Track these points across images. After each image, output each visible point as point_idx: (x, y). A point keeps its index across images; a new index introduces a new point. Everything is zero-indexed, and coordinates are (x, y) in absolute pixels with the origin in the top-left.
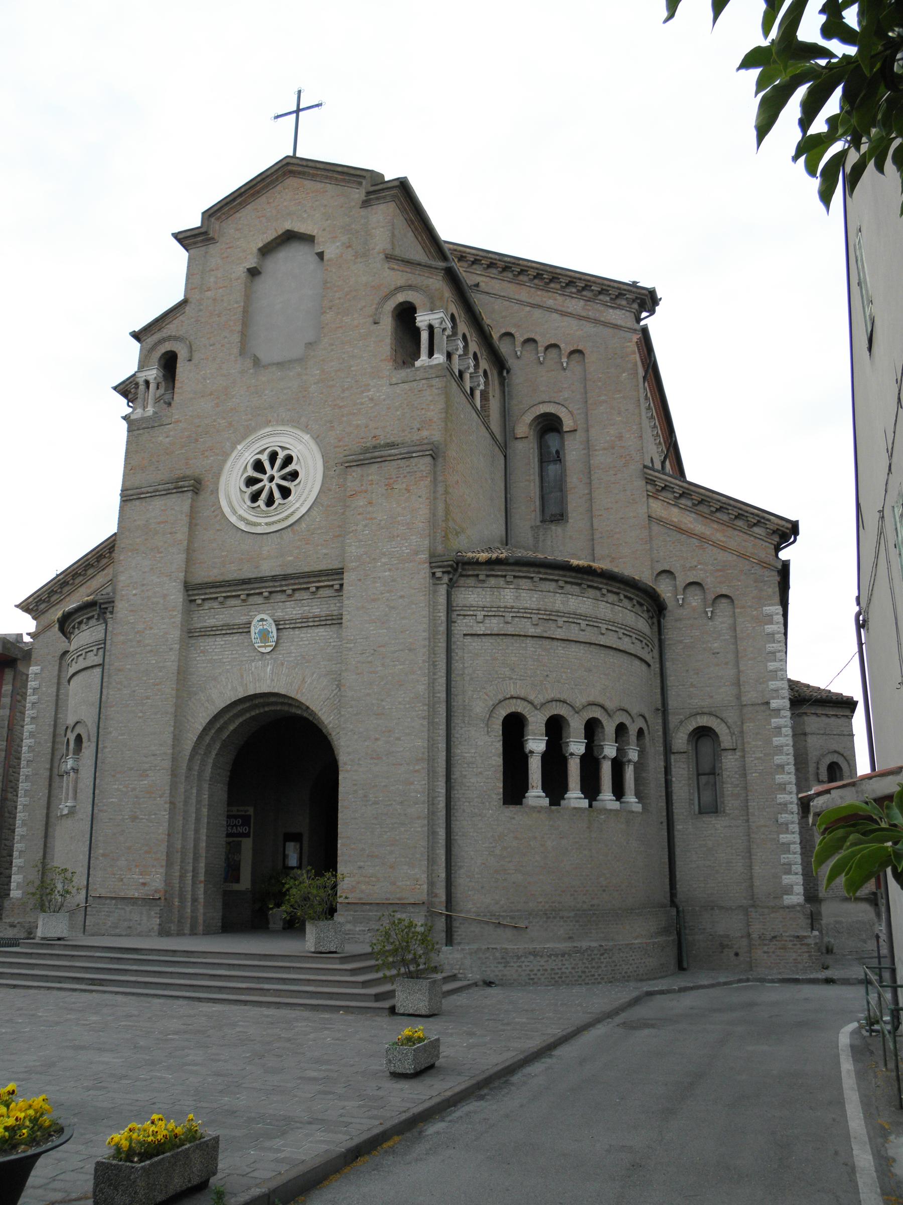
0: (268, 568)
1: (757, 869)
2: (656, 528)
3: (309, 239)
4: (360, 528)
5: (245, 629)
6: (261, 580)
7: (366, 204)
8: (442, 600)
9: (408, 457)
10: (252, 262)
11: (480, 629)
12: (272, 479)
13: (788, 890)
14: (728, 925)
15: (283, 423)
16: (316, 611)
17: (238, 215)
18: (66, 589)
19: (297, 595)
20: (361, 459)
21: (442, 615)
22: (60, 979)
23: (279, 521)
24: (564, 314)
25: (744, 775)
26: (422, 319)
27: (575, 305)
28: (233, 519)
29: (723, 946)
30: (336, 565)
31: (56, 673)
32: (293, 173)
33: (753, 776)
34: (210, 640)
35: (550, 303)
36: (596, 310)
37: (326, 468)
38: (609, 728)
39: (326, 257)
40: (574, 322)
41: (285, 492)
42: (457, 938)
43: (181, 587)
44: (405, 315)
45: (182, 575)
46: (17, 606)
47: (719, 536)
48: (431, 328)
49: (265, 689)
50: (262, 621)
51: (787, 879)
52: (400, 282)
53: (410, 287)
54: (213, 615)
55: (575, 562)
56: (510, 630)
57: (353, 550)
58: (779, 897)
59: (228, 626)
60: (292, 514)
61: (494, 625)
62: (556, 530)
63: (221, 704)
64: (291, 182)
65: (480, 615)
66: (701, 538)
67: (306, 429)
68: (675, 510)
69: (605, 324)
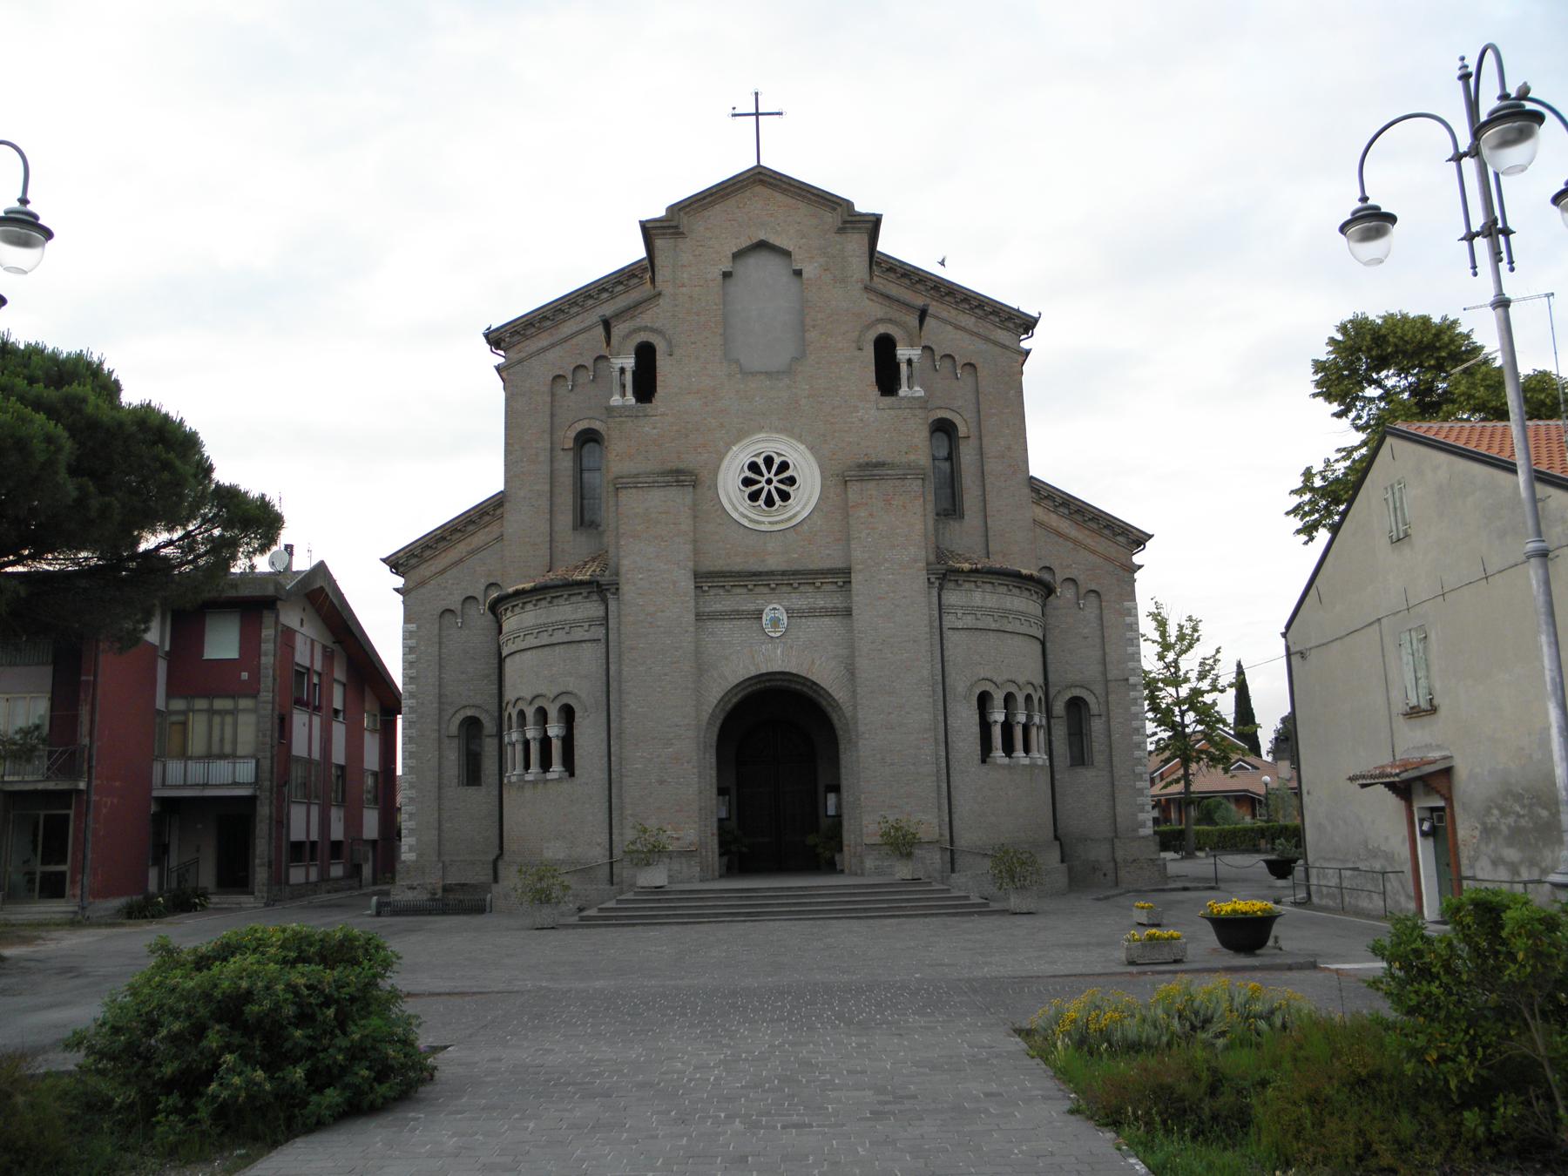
0: (773, 563)
1: (1119, 809)
2: (1038, 530)
3: (786, 254)
4: (863, 535)
5: (758, 615)
6: (771, 573)
7: (841, 230)
8: (935, 600)
9: (903, 478)
10: (727, 267)
11: (960, 624)
12: (769, 482)
13: (1143, 825)
14: (1099, 853)
15: (778, 430)
16: (821, 603)
17: (706, 213)
18: (441, 545)
19: (802, 588)
20: (856, 474)
21: (936, 613)
22: (716, 915)
23: (782, 521)
24: (957, 327)
25: (1109, 736)
26: (903, 353)
27: (968, 321)
28: (735, 515)
29: (1094, 869)
30: (840, 565)
31: (436, 632)
32: (762, 182)
33: (1115, 737)
34: (718, 623)
35: (944, 314)
36: (985, 328)
37: (823, 478)
38: (998, 698)
39: (805, 275)
40: (966, 336)
41: (785, 496)
42: (957, 867)
43: (690, 575)
44: (885, 348)
45: (691, 564)
46: (384, 560)
47: (1089, 541)
48: (910, 362)
49: (776, 669)
50: (774, 611)
51: (1141, 816)
52: (880, 315)
53: (890, 321)
54: (720, 602)
55: (1024, 571)
56: (980, 625)
57: (858, 554)
58: (1135, 830)
59: (738, 612)
60: (794, 516)
61: (969, 621)
62: (954, 525)
63: (734, 680)
64: (759, 189)
65: (960, 612)
66: (1075, 542)
67: (800, 439)
68: (1053, 516)
69: (996, 343)
